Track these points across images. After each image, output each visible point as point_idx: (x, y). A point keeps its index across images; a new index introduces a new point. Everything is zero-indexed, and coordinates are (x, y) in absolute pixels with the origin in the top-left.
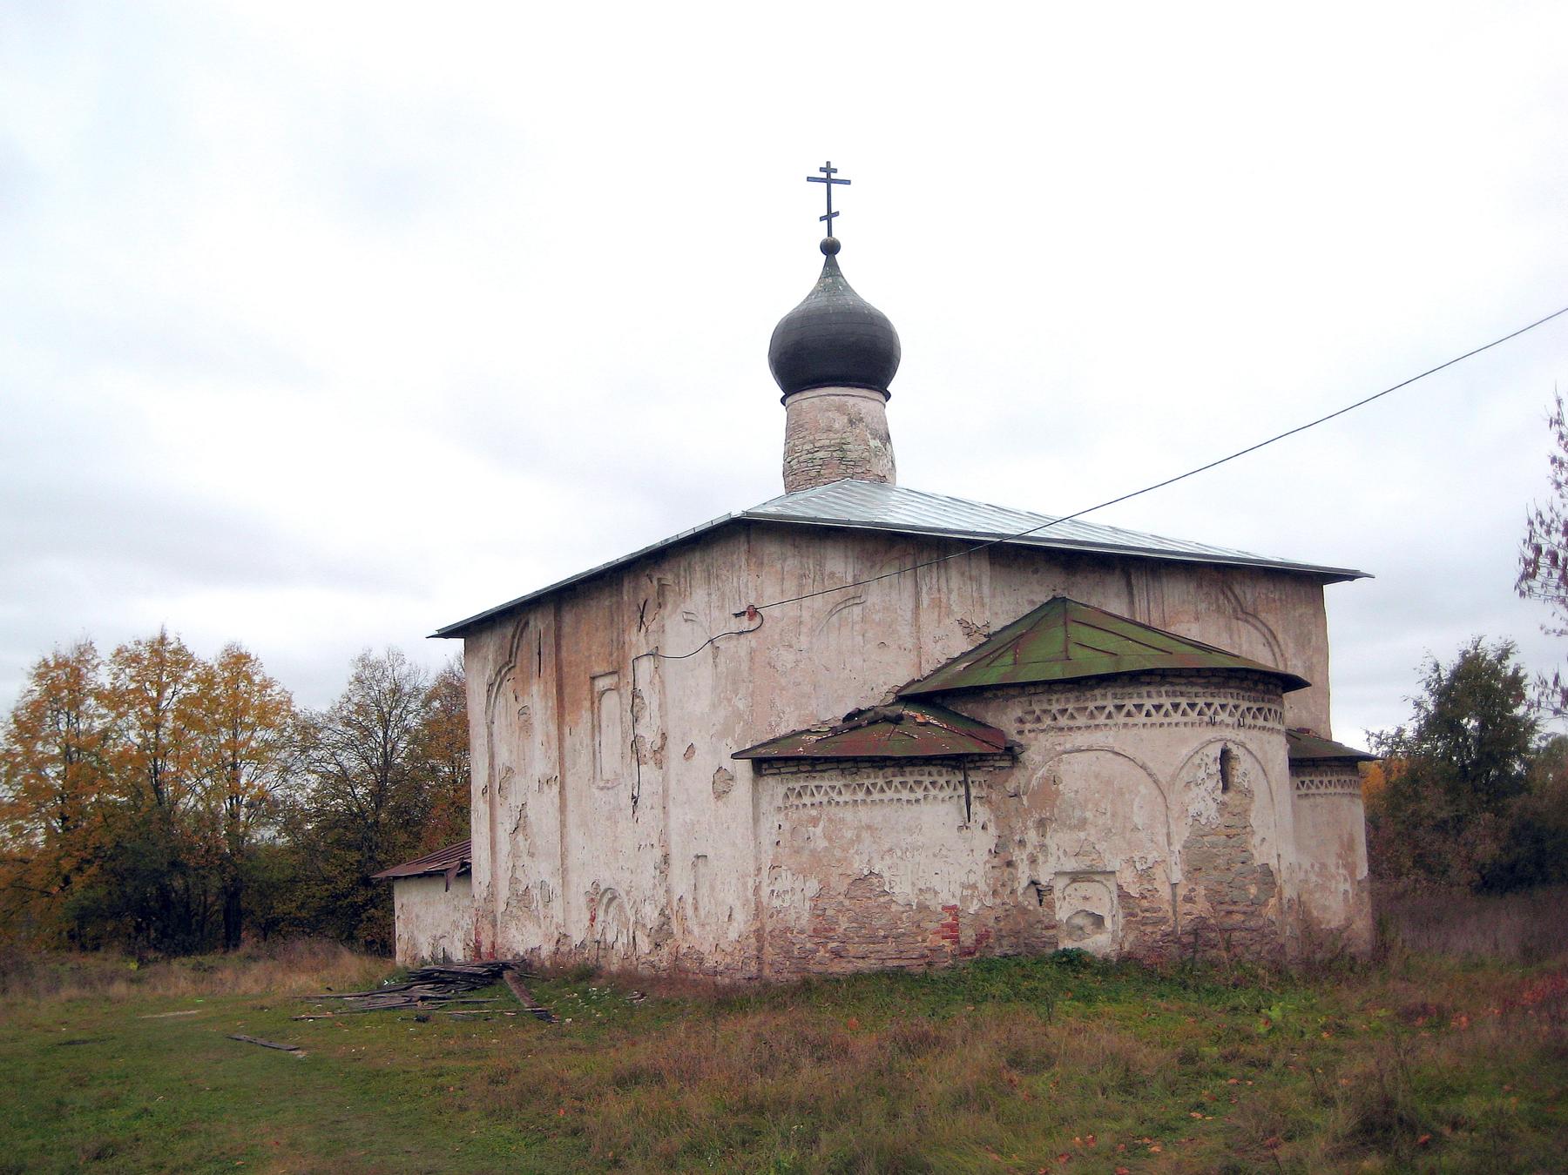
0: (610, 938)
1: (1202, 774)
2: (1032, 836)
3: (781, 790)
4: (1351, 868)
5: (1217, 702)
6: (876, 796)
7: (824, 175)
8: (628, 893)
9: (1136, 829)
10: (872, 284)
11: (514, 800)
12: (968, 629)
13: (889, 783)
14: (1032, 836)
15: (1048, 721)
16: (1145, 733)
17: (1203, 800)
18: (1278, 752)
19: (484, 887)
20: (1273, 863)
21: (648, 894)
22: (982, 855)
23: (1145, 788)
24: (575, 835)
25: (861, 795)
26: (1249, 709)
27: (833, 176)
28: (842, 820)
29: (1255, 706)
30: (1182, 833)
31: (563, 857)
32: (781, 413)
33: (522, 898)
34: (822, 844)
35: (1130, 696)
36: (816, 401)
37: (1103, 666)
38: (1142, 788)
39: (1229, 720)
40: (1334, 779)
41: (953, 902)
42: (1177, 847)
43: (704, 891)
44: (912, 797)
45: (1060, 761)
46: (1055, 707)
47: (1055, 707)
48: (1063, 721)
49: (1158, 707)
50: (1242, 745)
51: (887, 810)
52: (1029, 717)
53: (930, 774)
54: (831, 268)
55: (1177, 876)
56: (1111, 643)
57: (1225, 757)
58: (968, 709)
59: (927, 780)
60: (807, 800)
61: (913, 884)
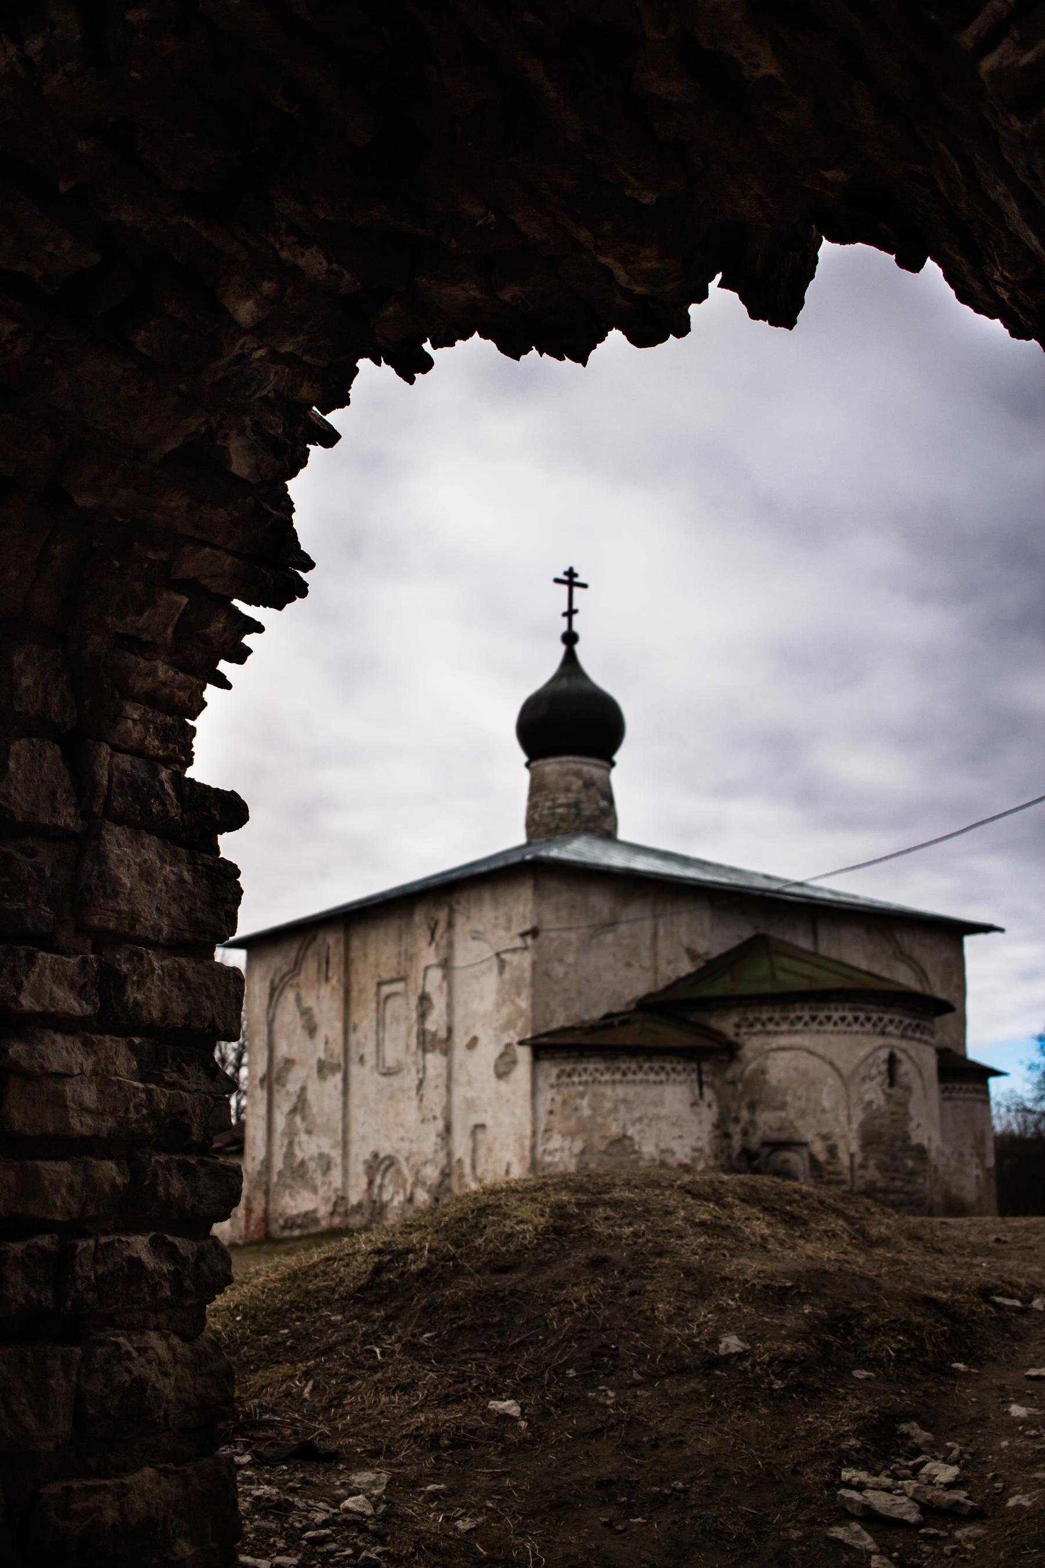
0: (386, 1197)
1: (874, 1071)
2: (745, 1114)
3: (555, 1071)
4: (982, 1157)
5: (887, 1017)
6: (630, 1077)
7: (566, 578)
8: (407, 1159)
9: (824, 1111)
10: (599, 669)
11: (293, 1087)
12: (692, 955)
13: (640, 1068)
14: (745, 1114)
15: (758, 1027)
16: (833, 1038)
17: (874, 1093)
18: (930, 1060)
19: (258, 1162)
20: (925, 1143)
21: (430, 1157)
22: (707, 1127)
23: (832, 1080)
24: (357, 1114)
25: (618, 1076)
26: (910, 1025)
27: (576, 580)
28: (603, 1095)
29: (914, 1022)
30: (859, 1116)
31: (346, 1130)
32: (525, 776)
33: (298, 1172)
34: (587, 1112)
35: (822, 1009)
36: (551, 766)
37: (802, 985)
38: (830, 1081)
39: (897, 1032)
40: (971, 1086)
41: (687, 1161)
42: (855, 1126)
43: (482, 1152)
44: (658, 1078)
45: (767, 1058)
46: (765, 1016)
47: (765, 1016)
48: (771, 1027)
49: (843, 1019)
50: (904, 1051)
51: (639, 1088)
52: (744, 1023)
53: (671, 1062)
54: (570, 660)
55: (854, 1147)
56: (807, 969)
57: (892, 1061)
58: (696, 1017)
59: (668, 1067)
60: (576, 1079)
61: (657, 1146)
